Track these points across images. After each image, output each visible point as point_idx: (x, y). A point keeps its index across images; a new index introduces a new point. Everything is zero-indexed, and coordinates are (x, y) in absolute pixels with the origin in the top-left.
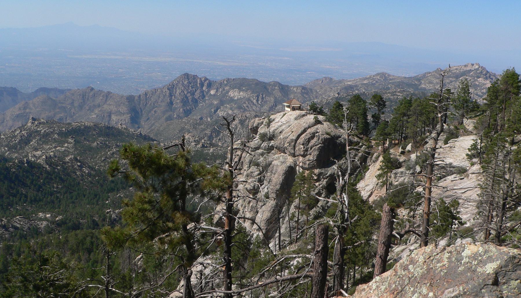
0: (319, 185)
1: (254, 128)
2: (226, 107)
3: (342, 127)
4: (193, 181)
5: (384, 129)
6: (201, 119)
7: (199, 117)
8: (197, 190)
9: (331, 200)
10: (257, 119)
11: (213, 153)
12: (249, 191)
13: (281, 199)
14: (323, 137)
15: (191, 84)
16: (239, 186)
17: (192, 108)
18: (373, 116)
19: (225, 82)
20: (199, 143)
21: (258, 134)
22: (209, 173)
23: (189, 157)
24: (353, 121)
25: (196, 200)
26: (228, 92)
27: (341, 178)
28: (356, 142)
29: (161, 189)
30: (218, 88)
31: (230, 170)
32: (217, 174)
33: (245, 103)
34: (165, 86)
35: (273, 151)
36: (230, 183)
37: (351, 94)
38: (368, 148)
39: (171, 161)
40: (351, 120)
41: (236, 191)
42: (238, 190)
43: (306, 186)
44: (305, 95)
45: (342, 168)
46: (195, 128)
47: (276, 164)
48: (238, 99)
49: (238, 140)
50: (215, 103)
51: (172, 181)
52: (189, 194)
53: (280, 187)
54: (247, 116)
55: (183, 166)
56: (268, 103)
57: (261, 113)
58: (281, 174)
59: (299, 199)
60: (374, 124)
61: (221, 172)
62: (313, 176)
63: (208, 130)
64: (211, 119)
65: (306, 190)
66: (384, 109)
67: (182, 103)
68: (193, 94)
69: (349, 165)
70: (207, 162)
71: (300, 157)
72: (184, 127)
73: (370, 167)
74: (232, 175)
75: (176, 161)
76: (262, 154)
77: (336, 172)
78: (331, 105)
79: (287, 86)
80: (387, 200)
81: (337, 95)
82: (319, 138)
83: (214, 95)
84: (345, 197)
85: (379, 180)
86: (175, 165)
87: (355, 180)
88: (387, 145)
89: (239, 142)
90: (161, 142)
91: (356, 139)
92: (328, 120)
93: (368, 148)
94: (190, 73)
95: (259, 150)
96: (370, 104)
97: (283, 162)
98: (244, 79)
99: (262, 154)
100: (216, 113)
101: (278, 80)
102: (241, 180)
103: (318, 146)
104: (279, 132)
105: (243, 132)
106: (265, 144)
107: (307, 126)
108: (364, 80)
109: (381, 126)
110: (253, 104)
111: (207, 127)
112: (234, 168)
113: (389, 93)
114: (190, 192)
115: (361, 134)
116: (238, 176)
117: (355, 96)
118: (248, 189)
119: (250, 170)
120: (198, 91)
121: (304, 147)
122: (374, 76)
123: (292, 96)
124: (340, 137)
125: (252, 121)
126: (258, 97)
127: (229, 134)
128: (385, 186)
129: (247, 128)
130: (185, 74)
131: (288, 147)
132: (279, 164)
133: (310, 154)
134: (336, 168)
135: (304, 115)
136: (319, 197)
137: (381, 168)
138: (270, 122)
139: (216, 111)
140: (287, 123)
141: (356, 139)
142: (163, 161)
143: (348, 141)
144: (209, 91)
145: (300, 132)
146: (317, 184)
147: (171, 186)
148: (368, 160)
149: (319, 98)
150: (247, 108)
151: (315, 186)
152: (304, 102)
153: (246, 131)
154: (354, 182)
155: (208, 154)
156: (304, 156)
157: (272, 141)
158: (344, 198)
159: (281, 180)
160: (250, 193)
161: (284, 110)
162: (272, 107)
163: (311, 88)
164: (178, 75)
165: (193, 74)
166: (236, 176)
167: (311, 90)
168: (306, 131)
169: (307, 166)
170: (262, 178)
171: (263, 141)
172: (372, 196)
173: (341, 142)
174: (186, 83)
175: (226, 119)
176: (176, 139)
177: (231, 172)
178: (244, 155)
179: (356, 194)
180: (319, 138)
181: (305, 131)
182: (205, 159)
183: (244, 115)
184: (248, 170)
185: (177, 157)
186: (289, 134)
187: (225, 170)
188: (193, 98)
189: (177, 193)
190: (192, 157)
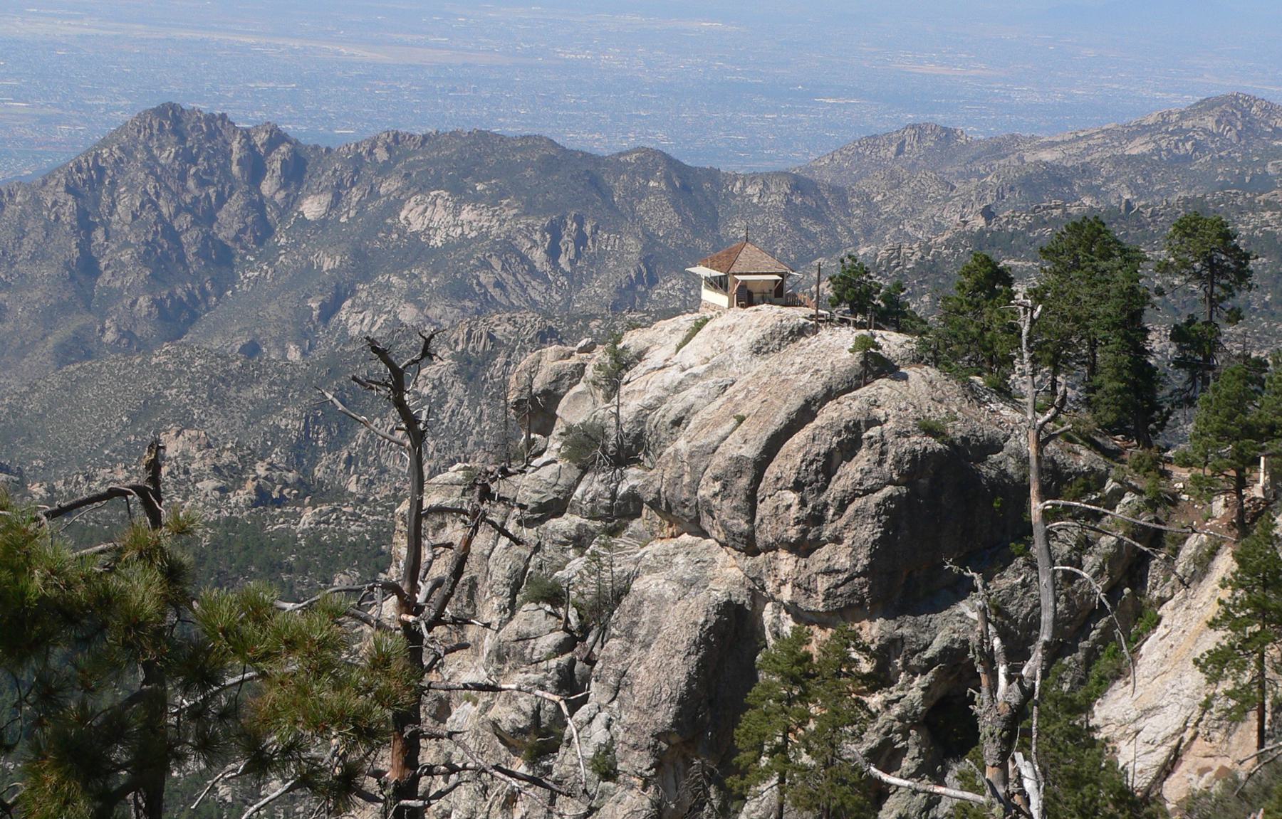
0: (888, 705)
1: (533, 398)
2: (388, 286)
3: (1005, 393)
4: (204, 689)
5: (1240, 403)
6: (252, 349)
7: (241, 341)
8: (227, 735)
9: (951, 791)
10: (551, 351)
11: (313, 536)
12: (511, 739)
13: (684, 783)
14: (906, 444)
15: (194, 161)
16: (455, 711)
17: (203, 289)
18: (1178, 335)
19: (381, 155)
20: (239, 482)
21: (555, 432)
22: (291, 645)
23: (187, 559)
24: (1067, 359)
25: (223, 790)
26: (394, 207)
27: (1002, 670)
28: (1085, 475)
29: (29, 735)
30: (340, 185)
31: (406, 625)
32: (335, 648)
33: (486, 265)
34: (52, 176)
35: (636, 525)
36: (406, 698)
37: (1056, 212)
38: (1152, 504)
39: (87, 579)
40: (1057, 356)
41: (439, 737)
42: (451, 735)
43: (814, 710)
44: (806, 223)
45: (1007, 616)
46: (221, 401)
47: (652, 591)
48: (449, 246)
49: (452, 463)
50: (328, 264)
51: (88, 690)
52: (181, 758)
53: (677, 715)
54: (498, 335)
55: (150, 607)
56: (611, 263)
57: (572, 320)
58: (682, 647)
59: (782, 781)
60: (1183, 374)
61: (360, 637)
62: (855, 655)
63: (291, 410)
64: (304, 354)
65: (814, 734)
66: (1240, 298)
67: (146, 263)
68: (206, 216)
69: (1047, 601)
70: (282, 584)
71: (783, 554)
72: (159, 396)
73: (1165, 611)
74: (416, 655)
75: (113, 580)
76: (579, 541)
77: (974, 638)
78: (948, 277)
79: (713, 175)
80: (1267, 793)
81: (980, 222)
82: (883, 453)
83: (322, 223)
84: (1027, 771)
85: (1214, 679)
86: (106, 601)
87: (1081, 682)
88: (1257, 491)
89: (455, 473)
90: (35, 479)
91: (1084, 458)
92: (930, 355)
93: (1152, 504)
94: (188, 105)
95: (559, 514)
96: (1165, 268)
97: (691, 583)
98: (483, 138)
99: (579, 541)
100: (334, 320)
101: (661, 140)
102: (468, 677)
103: (878, 496)
104: (668, 420)
105: (479, 420)
106: (591, 487)
107: (817, 388)
108: (1131, 137)
109: (1225, 386)
110: (532, 271)
111: (284, 395)
112: (430, 612)
113: (1269, 205)
114: (188, 749)
115: (1110, 429)
116: (449, 658)
117: (1077, 227)
118: (506, 726)
119: (514, 624)
120: (235, 203)
121: (803, 503)
122: (1183, 116)
123: (737, 229)
124: (994, 446)
125: (526, 362)
126: (555, 231)
127: (400, 434)
128: (1253, 716)
129: (496, 397)
130: (161, 111)
131: (716, 502)
132: (669, 591)
133: (837, 540)
134: (974, 616)
135: (801, 332)
136: (888, 772)
137: (1227, 615)
138: (622, 364)
139: (329, 310)
140: (710, 370)
141: (1084, 458)
142: (38, 581)
143: (1041, 471)
144: (292, 201)
145: (779, 419)
146: (875, 701)
147: (84, 715)
148: (1155, 571)
149: (881, 240)
150: (495, 292)
151: (863, 714)
152: (803, 259)
153: (492, 417)
154: (1079, 694)
155: (287, 540)
156: (802, 548)
157: (633, 471)
158: (1020, 777)
159: (680, 676)
160: (513, 749)
161: (693, 304)
162: (631, 286)
163: (838, 183)
164: (124, 117)
165: (205, 108)
166: (438, 657)
167: (840, 194)
168: (813, 416)
169: (817, 604)
170: (579, 666)
171: (584, 470)
172: (1181, 769)
173: (1003, 473)
174: (166, 156)
175: (383, 354)
176: (114, 462)
177: (412, 634)
178: (482, 541)
179: (1089, 756)
180: (883, 453)
181: (806, 413)
182: (273, 568)
183: (482, 329)
184: (502, 624)
185: (118, 560)
186: (721, 432)
187: (379, 625)
188: (208, 238)
189: (119, 754)
190: (201, 557)
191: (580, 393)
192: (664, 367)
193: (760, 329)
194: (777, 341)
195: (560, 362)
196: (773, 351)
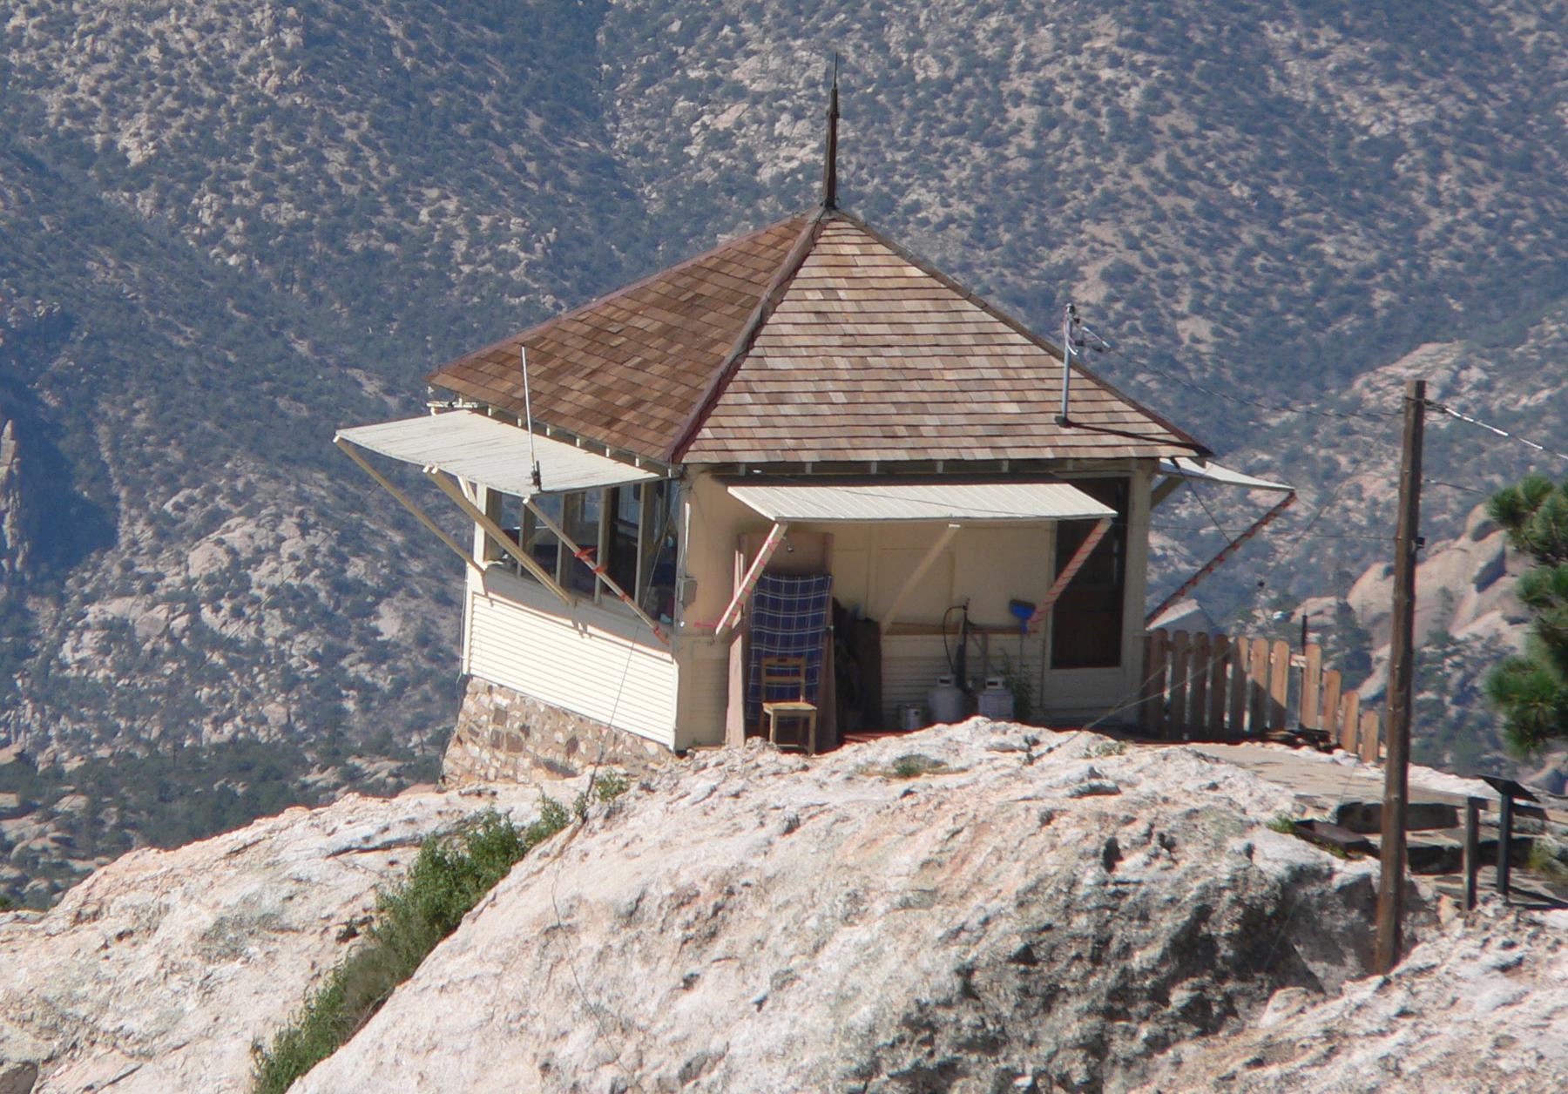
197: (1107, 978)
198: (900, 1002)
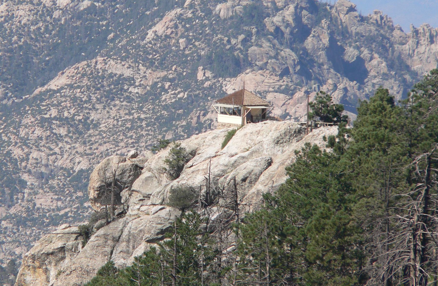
191: (149, 177)
192: (215, 156)
193: (278, 131)
194: (288, 137)
195: (122, 164)
196: (285, 142)
197: (290, 134)
198: (276, 136)
